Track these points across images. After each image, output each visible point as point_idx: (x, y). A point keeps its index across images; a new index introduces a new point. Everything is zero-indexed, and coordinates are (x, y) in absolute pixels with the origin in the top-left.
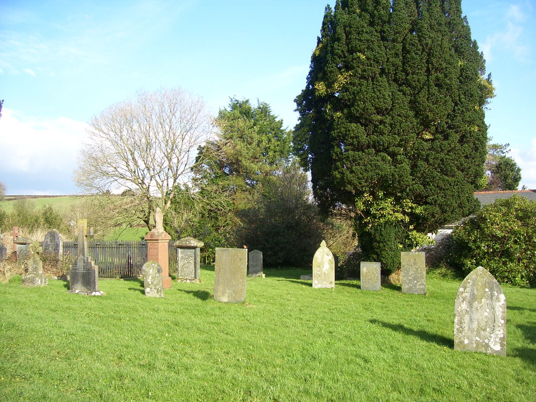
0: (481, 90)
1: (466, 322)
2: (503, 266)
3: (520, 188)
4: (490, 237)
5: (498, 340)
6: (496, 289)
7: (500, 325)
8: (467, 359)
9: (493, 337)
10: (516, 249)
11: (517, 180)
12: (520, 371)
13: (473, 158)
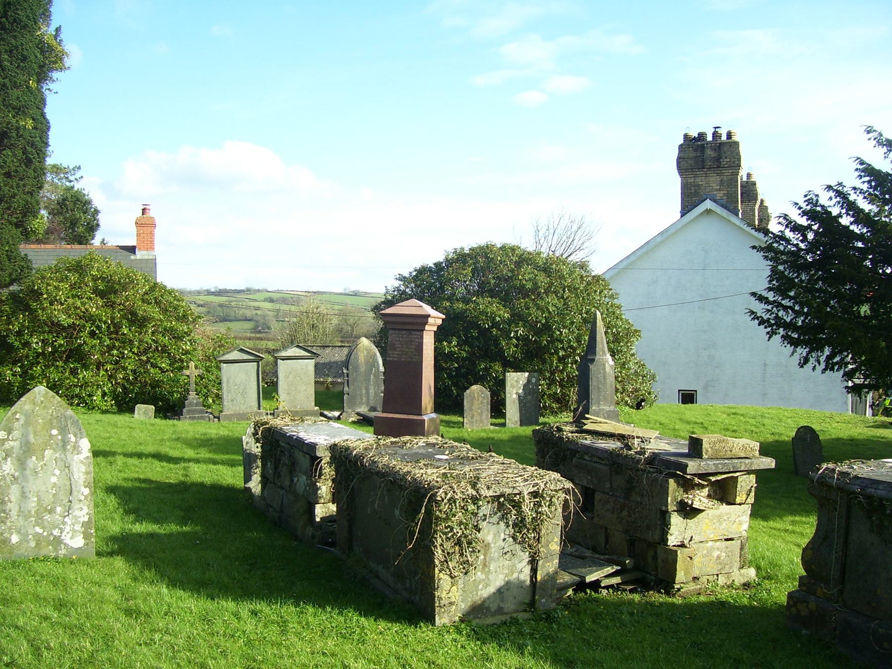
0: (42, 52)
1: (13, 499)
2: (72, 377)
3: (96, 242)
4: (47, 325)
5: (78, 527)
6: (72, 429)
7: (83, 498)
8: (20, 581)
9: (69, 523)
10: (94, 346)
11: (92, 228)
12: (128, 587)
13: (21, 179)
